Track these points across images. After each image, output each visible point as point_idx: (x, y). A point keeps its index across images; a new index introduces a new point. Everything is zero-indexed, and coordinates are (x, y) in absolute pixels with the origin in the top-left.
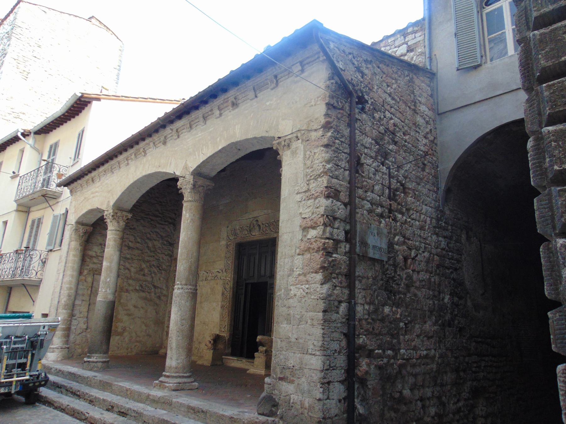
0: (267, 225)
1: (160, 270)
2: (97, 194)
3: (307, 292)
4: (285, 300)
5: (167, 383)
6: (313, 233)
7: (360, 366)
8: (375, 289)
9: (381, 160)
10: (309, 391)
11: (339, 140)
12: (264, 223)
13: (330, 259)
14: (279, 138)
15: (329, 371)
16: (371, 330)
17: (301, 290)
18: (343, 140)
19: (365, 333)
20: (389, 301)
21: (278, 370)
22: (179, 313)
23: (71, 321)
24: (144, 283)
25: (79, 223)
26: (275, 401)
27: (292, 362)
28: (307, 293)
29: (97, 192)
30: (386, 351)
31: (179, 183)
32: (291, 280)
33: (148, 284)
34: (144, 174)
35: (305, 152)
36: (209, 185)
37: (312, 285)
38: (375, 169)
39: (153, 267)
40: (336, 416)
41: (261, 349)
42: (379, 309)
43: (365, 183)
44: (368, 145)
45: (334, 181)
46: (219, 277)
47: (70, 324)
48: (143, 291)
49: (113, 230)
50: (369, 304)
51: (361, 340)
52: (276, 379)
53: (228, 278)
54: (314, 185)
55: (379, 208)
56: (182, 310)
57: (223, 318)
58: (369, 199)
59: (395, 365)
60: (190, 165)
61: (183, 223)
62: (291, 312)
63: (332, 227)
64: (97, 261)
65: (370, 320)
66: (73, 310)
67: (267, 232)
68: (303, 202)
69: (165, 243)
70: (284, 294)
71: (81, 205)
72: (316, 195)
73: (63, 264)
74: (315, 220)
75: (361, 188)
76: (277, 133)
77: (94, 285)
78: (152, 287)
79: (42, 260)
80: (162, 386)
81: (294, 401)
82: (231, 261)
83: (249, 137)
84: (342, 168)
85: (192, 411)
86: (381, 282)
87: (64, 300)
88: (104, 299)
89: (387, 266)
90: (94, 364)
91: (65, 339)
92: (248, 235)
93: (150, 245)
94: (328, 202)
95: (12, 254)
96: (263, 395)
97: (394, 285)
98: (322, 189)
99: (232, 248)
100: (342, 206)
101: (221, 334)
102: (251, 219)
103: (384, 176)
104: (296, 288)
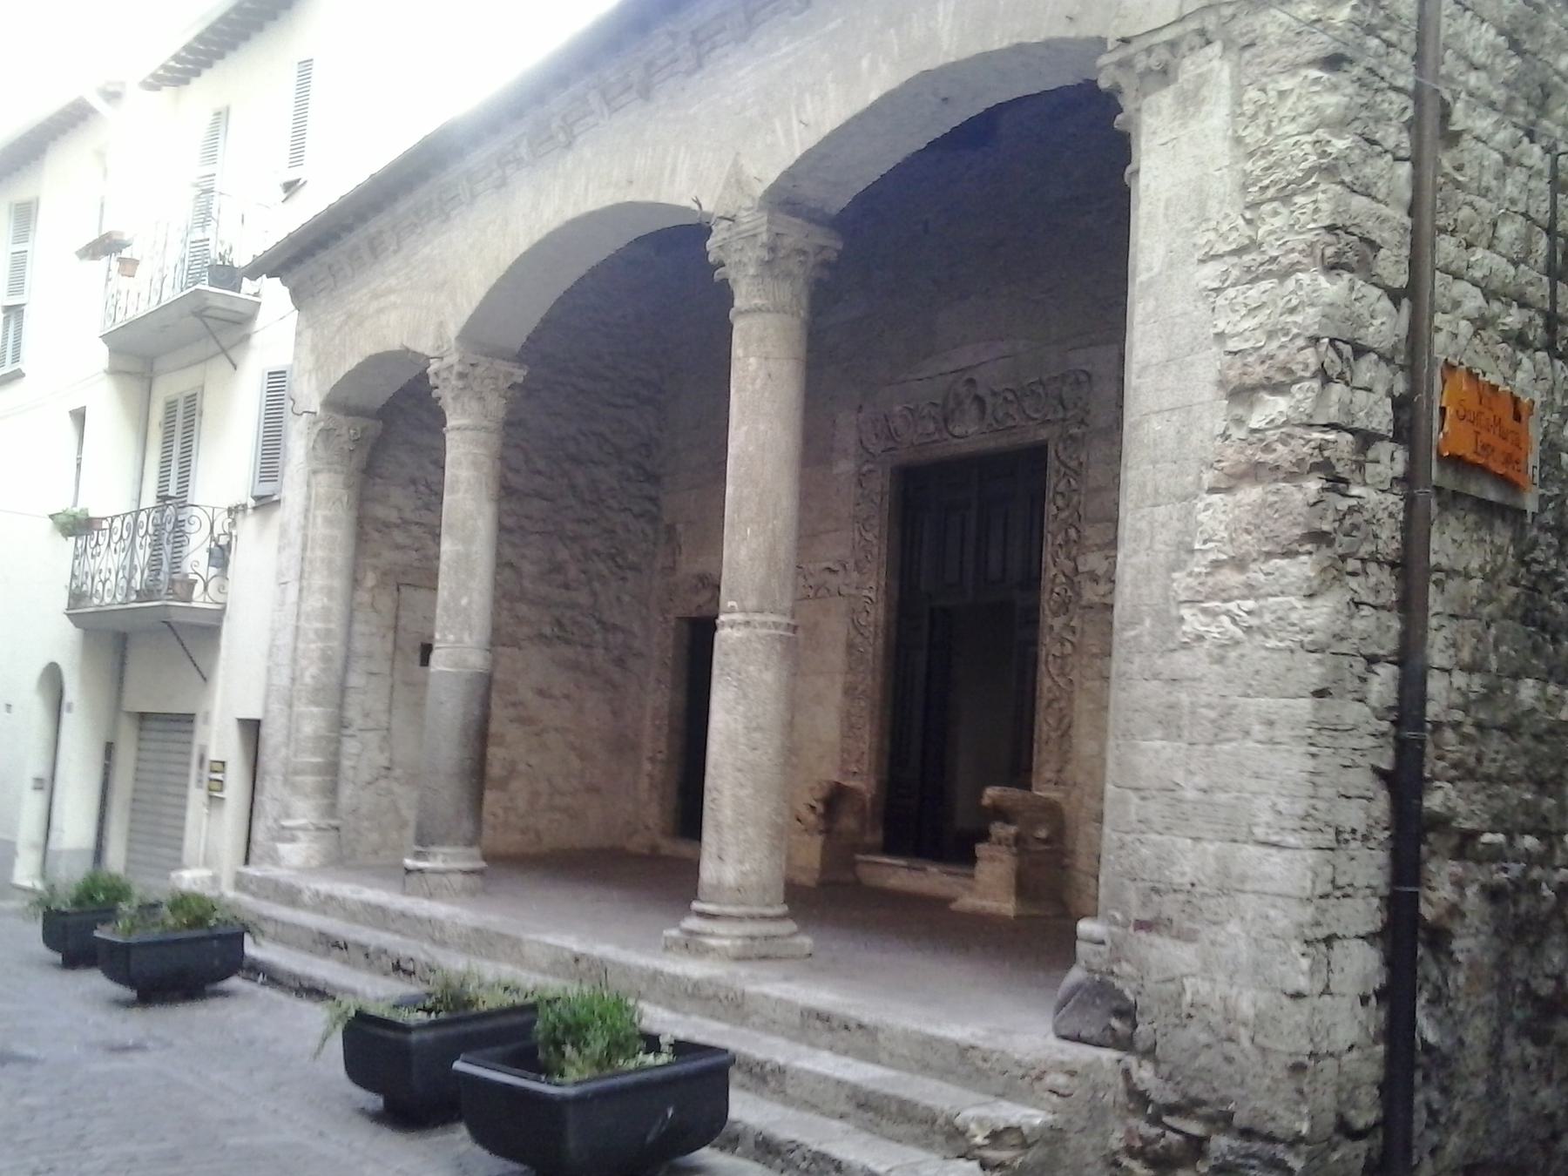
0: (1010, 397)
1: (619, 567)
2: (393, 298)
3: (1250, 627)
4: (1156, 655)
5: (712, 935)
6: (1275, 407)
7: (1430, 888)
8: (1490, 615)
9: (1525, 115)
10: (1257, 966)
11: (1378, 37)
12: (996, 389)
13: (1344, 504)
14: (1125, 41)
15: (1332, 901)
16: (1472, 761)
17: (1225, 620)
18: (1389, 35)
19: (1453, 773)
20: (1534, 662)
21: (1132, 896)
22: (741, 708)
23: (339, 742)
24: (569, 613)
25: (336, 403)
26: (1125, 999)
27: (1187, 869)
28: (1248, 630)
29: (391, 291)
30: (1517, 836)
31: (711, 244)
32: (1182, 582)
33: (580, 618)
34: (570, 213)
35: (1238, 90)
36: (823, 248)
37: (1271, 600)
38: (1503, 154)
39: (595, 558)
40: (1351, 1048)
41: (999, 830)
42: (1501, 689)
43: (1466, 212)
44: (1480, 56)
45: (1359, 203)
46: (833, 590)
47: (337, 753)
48: (568, 642)
49: (466, 428)
50: (1469, 669)
51: (1434, 801)
52: (1125, 926)
53: (866, 592)
54: (1278, 222)
55: (1514, 310)
56: (752, 696)
57: (852, 727)
58: (1478, 274)
59: (1544, 886)
60: (751, 170)
61: (737, 391)
62: (1184, 698)
63: (1347, 384)
64: (408, 542)
65: (1468, 729)
66: (341, 706)
67: (1010, 423)
68: (1231, 292)
69: (631, 471)
70: (1151, 634)
71: (337, 341)
72: (1285, 261)
73: (297, 550)
74: (1282, 356)
75: (1453, 233)
76: (1116, 22)
77: (402, 622)
78: (596, 627)
79: (215, 540)
80: (692, 945)
81: (1198, 999)
82: (876, 531)
83: (996, 47)
84: (1386, 151)
85: (818, 1024)
86: (1513, 591)
87: (311, 672)
88: (456, 665)
89: (1535, 532)
90: (436, 878)
91: (326, 801)
92: (936, 436)
93: (581, 480)
94: (1335, 287)
95: (117, 523)
96: (1076, 975)
97: (1553, 603)
98: (1309, 237)
99: (880, 483)
100: (1386, 304)
101: (846, 783)
102: (950, 378)
103: (1533, 184)
104: (1205, 611)
